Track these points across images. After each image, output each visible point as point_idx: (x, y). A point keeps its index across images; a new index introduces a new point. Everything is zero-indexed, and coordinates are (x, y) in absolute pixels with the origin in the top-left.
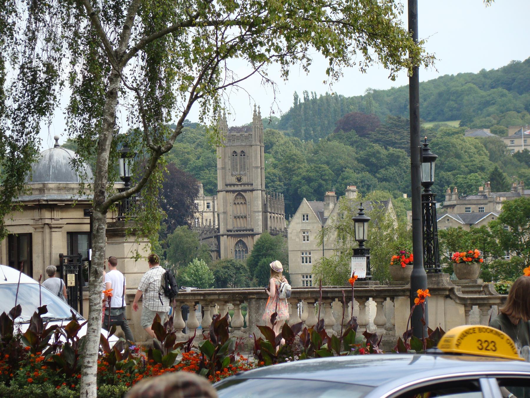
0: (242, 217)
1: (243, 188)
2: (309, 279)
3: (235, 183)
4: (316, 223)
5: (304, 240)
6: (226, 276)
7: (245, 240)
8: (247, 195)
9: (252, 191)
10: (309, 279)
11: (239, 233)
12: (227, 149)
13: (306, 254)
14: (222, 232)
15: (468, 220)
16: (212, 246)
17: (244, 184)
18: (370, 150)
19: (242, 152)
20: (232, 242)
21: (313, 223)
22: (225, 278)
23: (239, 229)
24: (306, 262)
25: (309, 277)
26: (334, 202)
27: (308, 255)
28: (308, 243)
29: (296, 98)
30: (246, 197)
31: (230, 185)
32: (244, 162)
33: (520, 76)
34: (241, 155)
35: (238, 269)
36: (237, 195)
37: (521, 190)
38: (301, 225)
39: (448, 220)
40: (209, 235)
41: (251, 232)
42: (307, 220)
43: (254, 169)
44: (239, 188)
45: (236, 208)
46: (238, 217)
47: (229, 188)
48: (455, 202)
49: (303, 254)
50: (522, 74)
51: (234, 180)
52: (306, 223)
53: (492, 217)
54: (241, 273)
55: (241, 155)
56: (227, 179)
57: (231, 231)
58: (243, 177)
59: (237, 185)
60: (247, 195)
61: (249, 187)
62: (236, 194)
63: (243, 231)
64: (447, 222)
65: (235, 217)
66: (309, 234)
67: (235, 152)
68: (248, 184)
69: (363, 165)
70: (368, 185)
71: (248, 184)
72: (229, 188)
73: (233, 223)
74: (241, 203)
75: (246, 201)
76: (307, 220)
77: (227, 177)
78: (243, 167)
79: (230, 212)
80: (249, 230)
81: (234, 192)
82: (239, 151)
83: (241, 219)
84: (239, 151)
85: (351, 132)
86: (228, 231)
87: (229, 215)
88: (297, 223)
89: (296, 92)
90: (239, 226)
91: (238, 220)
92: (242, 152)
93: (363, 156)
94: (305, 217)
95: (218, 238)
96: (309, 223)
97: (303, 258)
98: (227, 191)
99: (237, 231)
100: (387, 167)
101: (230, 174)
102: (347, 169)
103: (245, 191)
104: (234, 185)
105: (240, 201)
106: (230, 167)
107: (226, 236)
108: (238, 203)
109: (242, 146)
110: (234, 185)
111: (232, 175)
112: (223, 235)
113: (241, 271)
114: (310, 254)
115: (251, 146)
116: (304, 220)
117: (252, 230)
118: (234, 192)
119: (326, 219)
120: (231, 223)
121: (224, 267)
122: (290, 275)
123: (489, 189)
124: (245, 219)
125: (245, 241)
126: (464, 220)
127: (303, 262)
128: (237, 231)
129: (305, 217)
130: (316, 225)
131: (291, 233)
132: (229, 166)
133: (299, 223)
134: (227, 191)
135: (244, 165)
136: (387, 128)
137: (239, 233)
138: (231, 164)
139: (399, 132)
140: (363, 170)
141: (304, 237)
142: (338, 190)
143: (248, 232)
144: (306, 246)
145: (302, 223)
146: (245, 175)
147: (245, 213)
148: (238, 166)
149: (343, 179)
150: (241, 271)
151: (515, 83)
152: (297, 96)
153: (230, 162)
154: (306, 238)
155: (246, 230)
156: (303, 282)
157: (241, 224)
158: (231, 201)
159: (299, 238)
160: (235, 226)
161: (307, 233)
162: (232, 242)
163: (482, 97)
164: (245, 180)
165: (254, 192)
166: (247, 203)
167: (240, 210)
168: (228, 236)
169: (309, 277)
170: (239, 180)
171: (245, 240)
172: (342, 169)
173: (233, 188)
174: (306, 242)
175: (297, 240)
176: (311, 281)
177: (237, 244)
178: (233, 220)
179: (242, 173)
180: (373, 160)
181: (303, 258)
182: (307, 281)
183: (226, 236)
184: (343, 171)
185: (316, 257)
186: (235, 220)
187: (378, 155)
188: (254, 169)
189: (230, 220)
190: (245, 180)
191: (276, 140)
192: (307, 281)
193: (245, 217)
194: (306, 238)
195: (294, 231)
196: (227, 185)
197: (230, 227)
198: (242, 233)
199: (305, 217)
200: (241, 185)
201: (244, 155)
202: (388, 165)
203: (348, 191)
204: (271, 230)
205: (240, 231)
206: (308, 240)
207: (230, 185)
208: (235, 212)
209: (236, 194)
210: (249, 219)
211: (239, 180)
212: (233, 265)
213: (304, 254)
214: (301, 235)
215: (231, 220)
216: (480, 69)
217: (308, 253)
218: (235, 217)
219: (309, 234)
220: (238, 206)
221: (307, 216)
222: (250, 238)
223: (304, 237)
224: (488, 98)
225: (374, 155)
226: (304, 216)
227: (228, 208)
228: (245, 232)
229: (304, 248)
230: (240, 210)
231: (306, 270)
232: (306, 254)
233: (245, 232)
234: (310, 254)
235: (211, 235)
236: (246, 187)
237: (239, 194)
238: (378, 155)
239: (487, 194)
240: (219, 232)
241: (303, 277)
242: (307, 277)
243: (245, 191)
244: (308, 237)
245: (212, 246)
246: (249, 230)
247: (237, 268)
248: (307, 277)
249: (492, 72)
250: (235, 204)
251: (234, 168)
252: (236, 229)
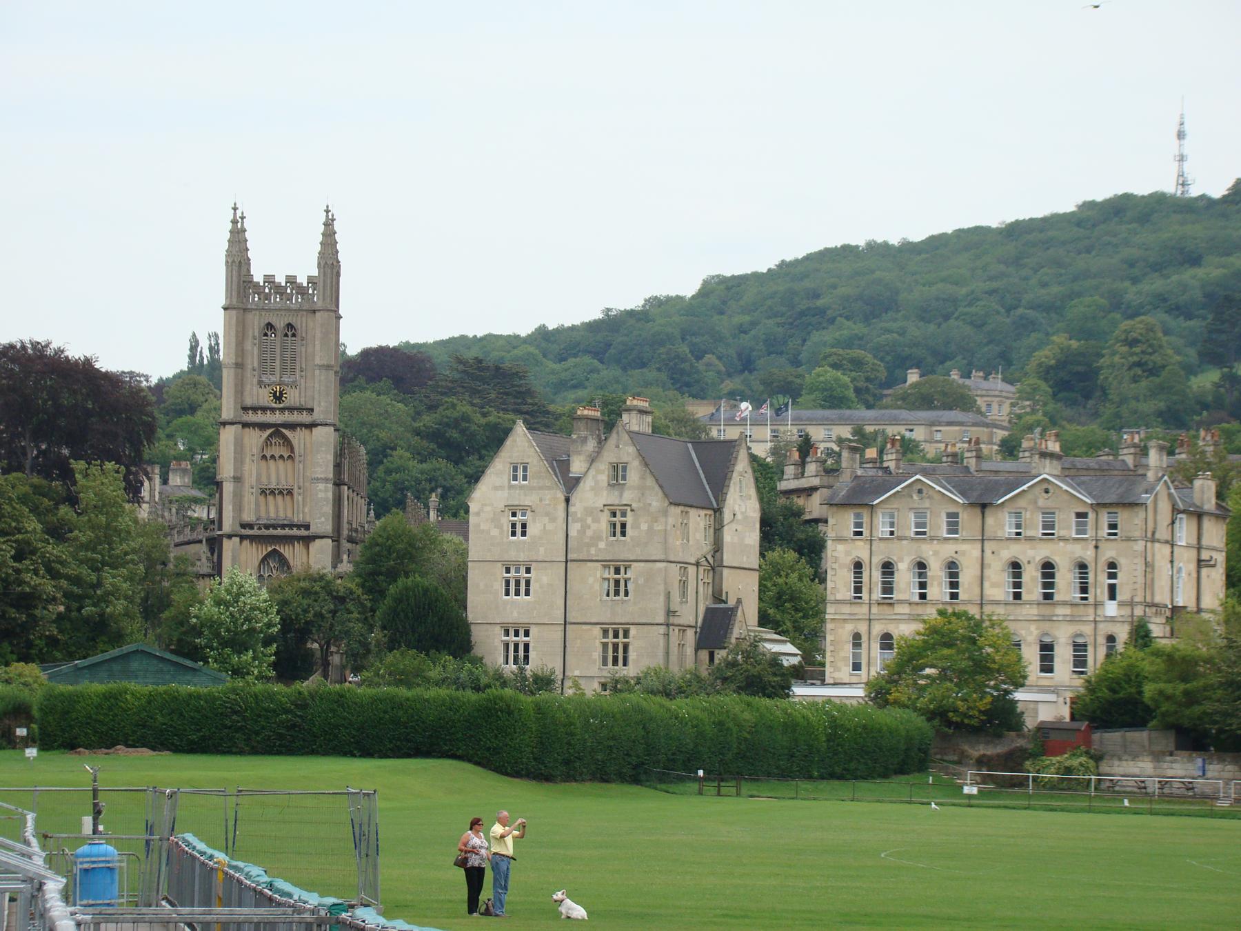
0: (281, 493)
1: (287, 417)
2: (522, 638)
3: (266, 404)
4: (549, 488)
5: (514, 534)
6: (310, 616)
7: (286, 551)
8: (296, 437)
9: (311, 426)
10: (522, 638)
11: (272, 532)
12: (249, 316)
13: (517, 571)
14: (227, 527)
15: (975, 494)
16: (198, 563)
17: (291, 409)
18: (448, 413)
19: (290, 326)
20: (253, 554)
21: (540, 488)
22: (307, 623)
23: (272, 522)
24: (517, 593)
25: (522, 633)
26: (599, 436)
27: (523, 574)
28: (524, 542)
29: (194, 346)
30: (295, 442)
31: (254, 409)
32: (294, 352)
33: (621, 339)
34: (286, 335)
35: (342, 600)
36: (271, 435)
37: (973, 461)
38: (506, 493)
39: (920, 491)
40: (188, 535)
41: (303, 532)
42: (525, 479)
43: (317, 372)
44: (277, 418)
45: (268, 468)
46: (272, 492)
47: (251, 417)
48: (816, 482)
49: (508, 571)
50: (627, 335)
51: (265, 398)
52: (522, 487)
53: (1045, 486)
54: (350, 612)
55: (286, 335)
56: (247, 393)
57: (251, 526)
58: (287, 390)
59: (273, 410)
60: (296, 437)
61: (305, 418)
62: (269, 431)
63: (283, 527)
64: (915, 497)
65: (263, 492)
66: (528, 517)
67: (270, 326)
68: (300, 409)
69: (433, 446)
70: (444, 487)
71: (300, 409)
72: (251, 417)
73: (257, 504)
74: (281, 457)
75: (292, 450)
76: (525, 479)
77: (248, 388)
78: (289, 366)
79: (250, 478)
80: (299, 527)
81: (262, 426)
82: (280, 323)
83: (279, 498)
84: (280, 323)
85: (382, 384)
86: (243, 526)
87: (247, 485)
88: (496, 488)
89: (194, 335)
90: (272, 515)
91: (270, 498)
92: (290, 326)
93: (430, 424)
94: (519, 471)
95: (215, 544)
96: (531, 488)
97: (508, 583)
98: (246, 425)
99: (267, 527)
100: (484, 452)
101: (255, 381)
102: (399, 451)
103: (292, 426)
104: (264, 409)
105: (277, 451)
106: (256, 365)
107: (237, 539)
108: (273, 457)
109: (289, 310)
110: (264, 409)
111: (260, 384)
112: (230, 537)
113: (350, 606)
114: (528, 571)
115: (314, 312)
116: (515, 479)
117: (307, 527)
118: (262, 426)
119: (578, 480)
120: (253, 506)
121: (306, 593)
122: (473, 627)
123: (897, 452)
124: (288, 498)
125: (286, 555)
126: (963, 494)
127: (507, 593)
128: (267, 527)
129: (520, 473)
130: (548, 496)
131: (478, 514)
132: (252, 361)
133: (501, 488)
134: (246, 425)
135: (293, 360)
136: (452, 382)
137: (272, 532)
138: (259, 356)
139: (479, 392)
140: (432, 454)
141: (514, 525)
142: (376, 495)
143: (295, 532)
144: (517, 548)
145: (511, 487)
146: (294, 385)
147: (291, 481)
148: (278, 363)
149: (389, 472)
150: (350, 606)
151: (612, 351)
152: (197, 342)
153: (256, 351)
154: (519, 530)
155: (291, 526)
156: (507, 645)
157: (277, 509)
158: (255, 451)
159: (500, 527)
160: (263, 514)
161: (523, 515)
162: (253, 554)
163: (553, 372)
164: (292, 397)
165: (316, 431)
166: (297, 459)
167: (278, 473)
168: (242, 538)
169: (522, 633)
170: (278, 397)
171: (286, 551)
172: (384, 450)
173: (260, 417)
174: (519, 537)
175: (495, 532)
176: (527, 646)
177: (264, 560)
178: (257, 500)
179: (285, 379)
180: (454, 434)
181: (508, 583)
182: (516, 646)
183: (237, 539)
184: (386, 456)
185: (545, 580)
186: (262, 498)
187: (464, 425)
188: (317, 372)
189: (250, 499)
190: (292, 397)
191: (202, 399)
192: (516, 646)
193: (290, 493)
194: (519, 530)
195: (488, 509)
196: (245, 409)
197: (248, 517)
198: (279, 532)
199: (520, 473)
200: (282, 410)
201: (294, 335)
202: (485, 447)
203: (629, 410)
204: (351, 530)
205: (275, 527)
206: (524, 534)
207: (254, 409)
208: (264, 479)
209: (269, 431)
210: (298, 498)
211: (278, 397)
212: (328, 587)
213: (513, 570)
214: (507, 520)
215: (253, 499)
216: (537, 326)
217: (523, 569)
218: (263, 492)
219: (528, 517)
220: (272, 462)
221: (525, 469)
222: (299, 547)
223: (514, 525)
224: (563, 375)
225: (456, 423)
226: (515, 469)
227: (247, 467)
228: (287, 532)
229: (512, 555)
230: (278, 473)
231: (515, 614)
232: (517, 571)
233: (287, 532)
234: (528, 571)
235: (194, 536)
236: (295, 417)
237: (277, 432)
238: (464, 425)
239: (892, 465)
240: (220, 528)
241: (507, 633)
242: (517, 634)
243: (292, 426)
244: (524, 526)
245: (198, 563)
246: (299, 527)
247: (335, 598)
248: (517, 634)
249: (559, 331)
250: (264, 457)
251: (264, 366)
252: (265, 522)
